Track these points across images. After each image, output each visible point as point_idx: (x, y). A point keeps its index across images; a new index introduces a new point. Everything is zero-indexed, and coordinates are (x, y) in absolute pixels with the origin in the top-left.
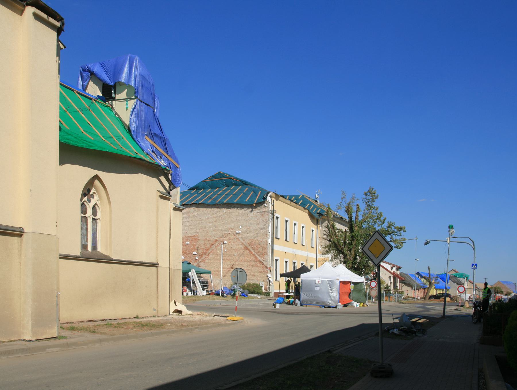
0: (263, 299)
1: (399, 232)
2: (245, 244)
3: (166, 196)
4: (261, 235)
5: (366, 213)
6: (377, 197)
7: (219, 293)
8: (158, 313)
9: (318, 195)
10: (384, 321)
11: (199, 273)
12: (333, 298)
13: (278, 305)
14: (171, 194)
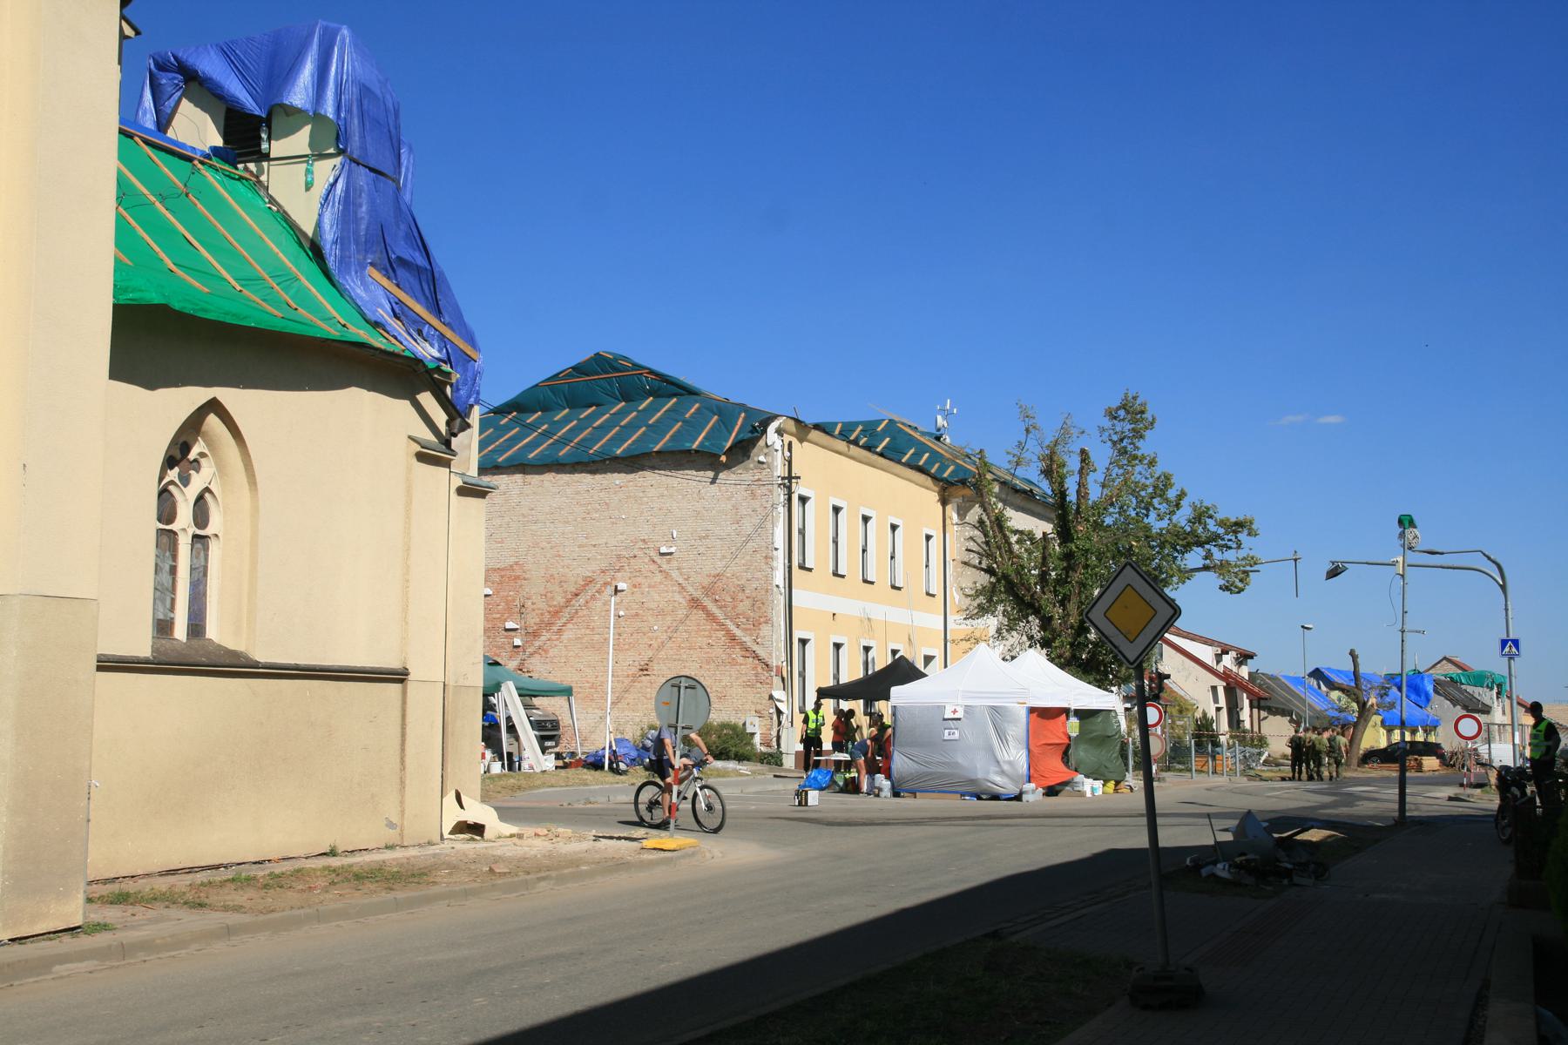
0: (759, 777)
1: (1233, 538)
2: (690, 589)
3: (435, 455)
4: (748, 558)
5: (1114, 476)
6: (1152, 424)
7: (601, 760)
8: (401, 835)
9: (944, 420)
10: (1167, 839)
11: (527, 694)
12: (1006, 767)
13: (813, 797)
14: (453, 447)
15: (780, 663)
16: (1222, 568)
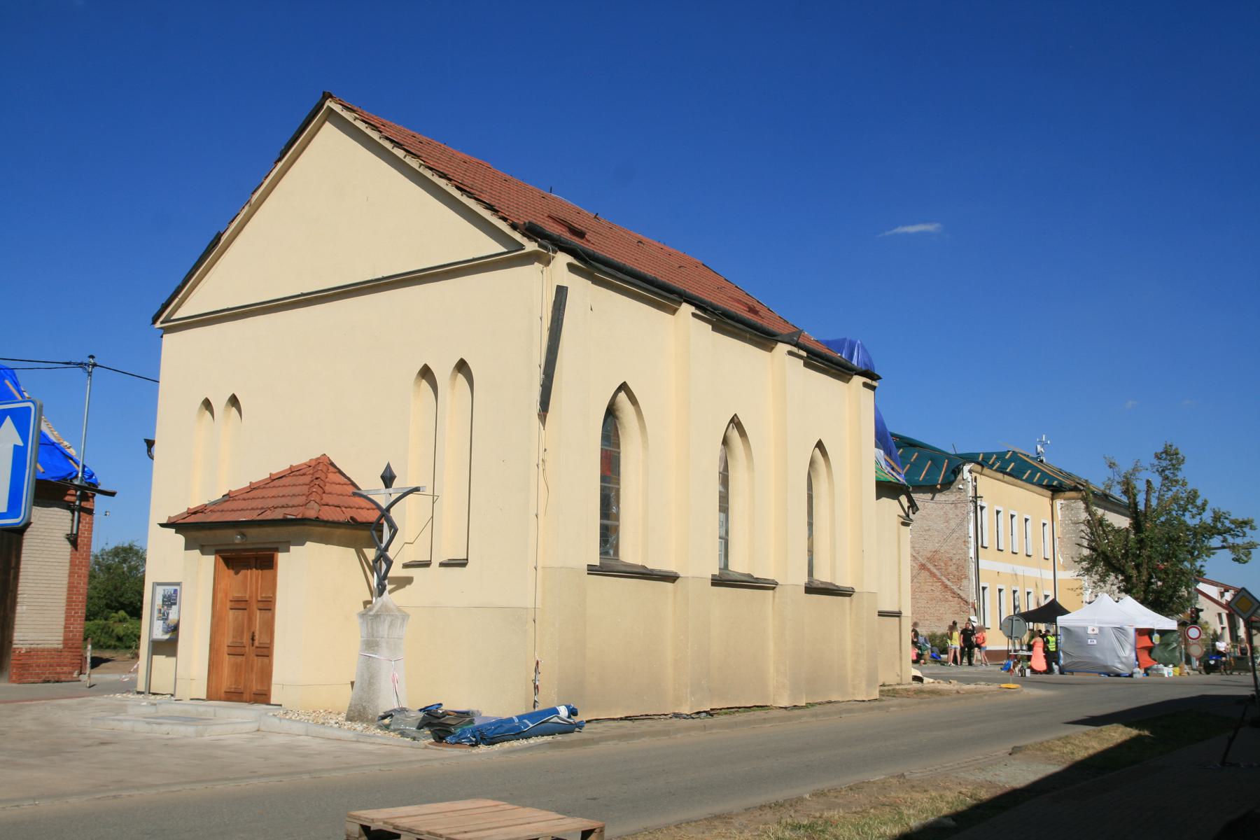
4: (954, 542)
6: (1183, 460)
12: (1124, 660)
16: (1233, 548)
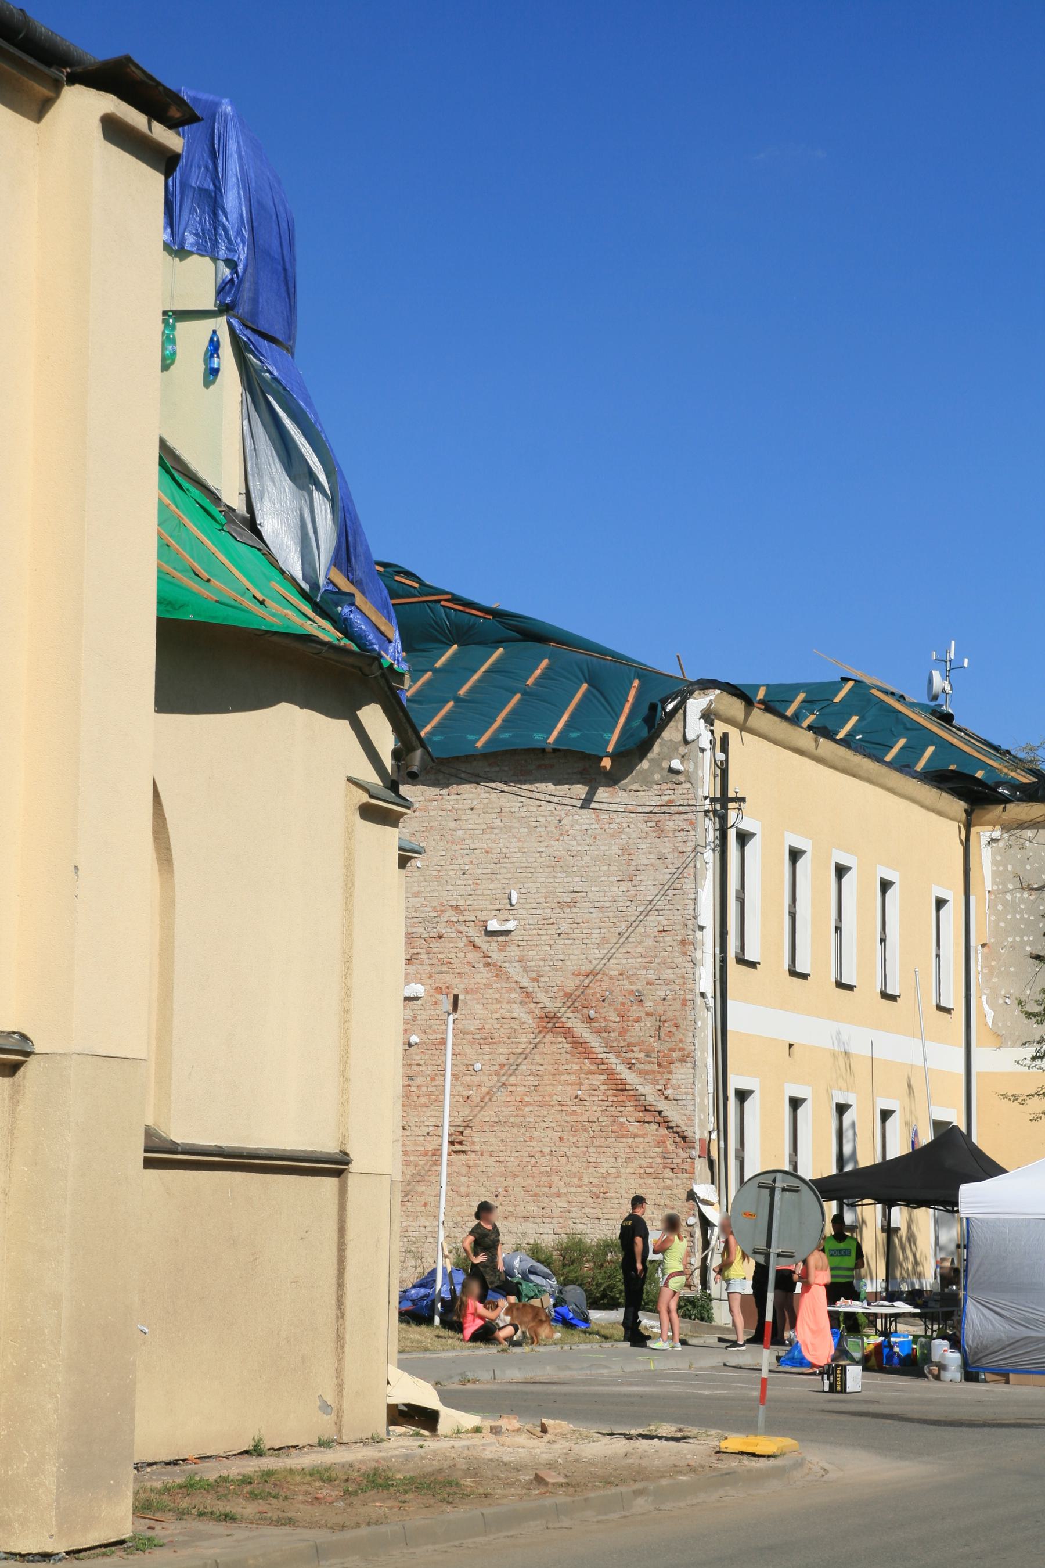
2: (542, 997)
4: (650, 942)
8: (339, 1425)
15: (706, 1134)
